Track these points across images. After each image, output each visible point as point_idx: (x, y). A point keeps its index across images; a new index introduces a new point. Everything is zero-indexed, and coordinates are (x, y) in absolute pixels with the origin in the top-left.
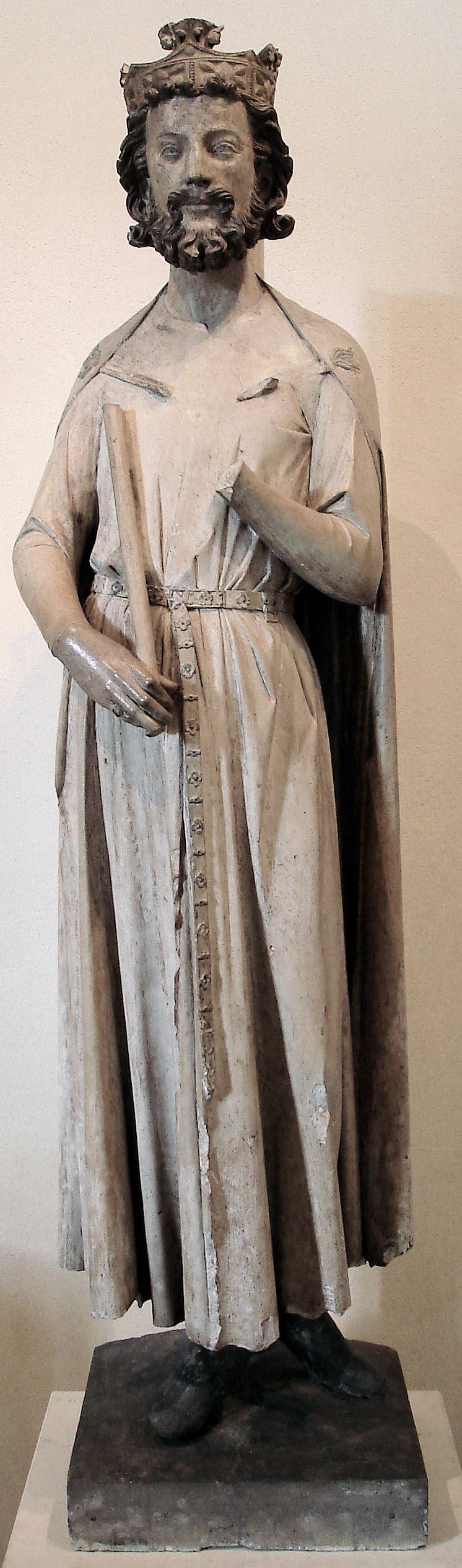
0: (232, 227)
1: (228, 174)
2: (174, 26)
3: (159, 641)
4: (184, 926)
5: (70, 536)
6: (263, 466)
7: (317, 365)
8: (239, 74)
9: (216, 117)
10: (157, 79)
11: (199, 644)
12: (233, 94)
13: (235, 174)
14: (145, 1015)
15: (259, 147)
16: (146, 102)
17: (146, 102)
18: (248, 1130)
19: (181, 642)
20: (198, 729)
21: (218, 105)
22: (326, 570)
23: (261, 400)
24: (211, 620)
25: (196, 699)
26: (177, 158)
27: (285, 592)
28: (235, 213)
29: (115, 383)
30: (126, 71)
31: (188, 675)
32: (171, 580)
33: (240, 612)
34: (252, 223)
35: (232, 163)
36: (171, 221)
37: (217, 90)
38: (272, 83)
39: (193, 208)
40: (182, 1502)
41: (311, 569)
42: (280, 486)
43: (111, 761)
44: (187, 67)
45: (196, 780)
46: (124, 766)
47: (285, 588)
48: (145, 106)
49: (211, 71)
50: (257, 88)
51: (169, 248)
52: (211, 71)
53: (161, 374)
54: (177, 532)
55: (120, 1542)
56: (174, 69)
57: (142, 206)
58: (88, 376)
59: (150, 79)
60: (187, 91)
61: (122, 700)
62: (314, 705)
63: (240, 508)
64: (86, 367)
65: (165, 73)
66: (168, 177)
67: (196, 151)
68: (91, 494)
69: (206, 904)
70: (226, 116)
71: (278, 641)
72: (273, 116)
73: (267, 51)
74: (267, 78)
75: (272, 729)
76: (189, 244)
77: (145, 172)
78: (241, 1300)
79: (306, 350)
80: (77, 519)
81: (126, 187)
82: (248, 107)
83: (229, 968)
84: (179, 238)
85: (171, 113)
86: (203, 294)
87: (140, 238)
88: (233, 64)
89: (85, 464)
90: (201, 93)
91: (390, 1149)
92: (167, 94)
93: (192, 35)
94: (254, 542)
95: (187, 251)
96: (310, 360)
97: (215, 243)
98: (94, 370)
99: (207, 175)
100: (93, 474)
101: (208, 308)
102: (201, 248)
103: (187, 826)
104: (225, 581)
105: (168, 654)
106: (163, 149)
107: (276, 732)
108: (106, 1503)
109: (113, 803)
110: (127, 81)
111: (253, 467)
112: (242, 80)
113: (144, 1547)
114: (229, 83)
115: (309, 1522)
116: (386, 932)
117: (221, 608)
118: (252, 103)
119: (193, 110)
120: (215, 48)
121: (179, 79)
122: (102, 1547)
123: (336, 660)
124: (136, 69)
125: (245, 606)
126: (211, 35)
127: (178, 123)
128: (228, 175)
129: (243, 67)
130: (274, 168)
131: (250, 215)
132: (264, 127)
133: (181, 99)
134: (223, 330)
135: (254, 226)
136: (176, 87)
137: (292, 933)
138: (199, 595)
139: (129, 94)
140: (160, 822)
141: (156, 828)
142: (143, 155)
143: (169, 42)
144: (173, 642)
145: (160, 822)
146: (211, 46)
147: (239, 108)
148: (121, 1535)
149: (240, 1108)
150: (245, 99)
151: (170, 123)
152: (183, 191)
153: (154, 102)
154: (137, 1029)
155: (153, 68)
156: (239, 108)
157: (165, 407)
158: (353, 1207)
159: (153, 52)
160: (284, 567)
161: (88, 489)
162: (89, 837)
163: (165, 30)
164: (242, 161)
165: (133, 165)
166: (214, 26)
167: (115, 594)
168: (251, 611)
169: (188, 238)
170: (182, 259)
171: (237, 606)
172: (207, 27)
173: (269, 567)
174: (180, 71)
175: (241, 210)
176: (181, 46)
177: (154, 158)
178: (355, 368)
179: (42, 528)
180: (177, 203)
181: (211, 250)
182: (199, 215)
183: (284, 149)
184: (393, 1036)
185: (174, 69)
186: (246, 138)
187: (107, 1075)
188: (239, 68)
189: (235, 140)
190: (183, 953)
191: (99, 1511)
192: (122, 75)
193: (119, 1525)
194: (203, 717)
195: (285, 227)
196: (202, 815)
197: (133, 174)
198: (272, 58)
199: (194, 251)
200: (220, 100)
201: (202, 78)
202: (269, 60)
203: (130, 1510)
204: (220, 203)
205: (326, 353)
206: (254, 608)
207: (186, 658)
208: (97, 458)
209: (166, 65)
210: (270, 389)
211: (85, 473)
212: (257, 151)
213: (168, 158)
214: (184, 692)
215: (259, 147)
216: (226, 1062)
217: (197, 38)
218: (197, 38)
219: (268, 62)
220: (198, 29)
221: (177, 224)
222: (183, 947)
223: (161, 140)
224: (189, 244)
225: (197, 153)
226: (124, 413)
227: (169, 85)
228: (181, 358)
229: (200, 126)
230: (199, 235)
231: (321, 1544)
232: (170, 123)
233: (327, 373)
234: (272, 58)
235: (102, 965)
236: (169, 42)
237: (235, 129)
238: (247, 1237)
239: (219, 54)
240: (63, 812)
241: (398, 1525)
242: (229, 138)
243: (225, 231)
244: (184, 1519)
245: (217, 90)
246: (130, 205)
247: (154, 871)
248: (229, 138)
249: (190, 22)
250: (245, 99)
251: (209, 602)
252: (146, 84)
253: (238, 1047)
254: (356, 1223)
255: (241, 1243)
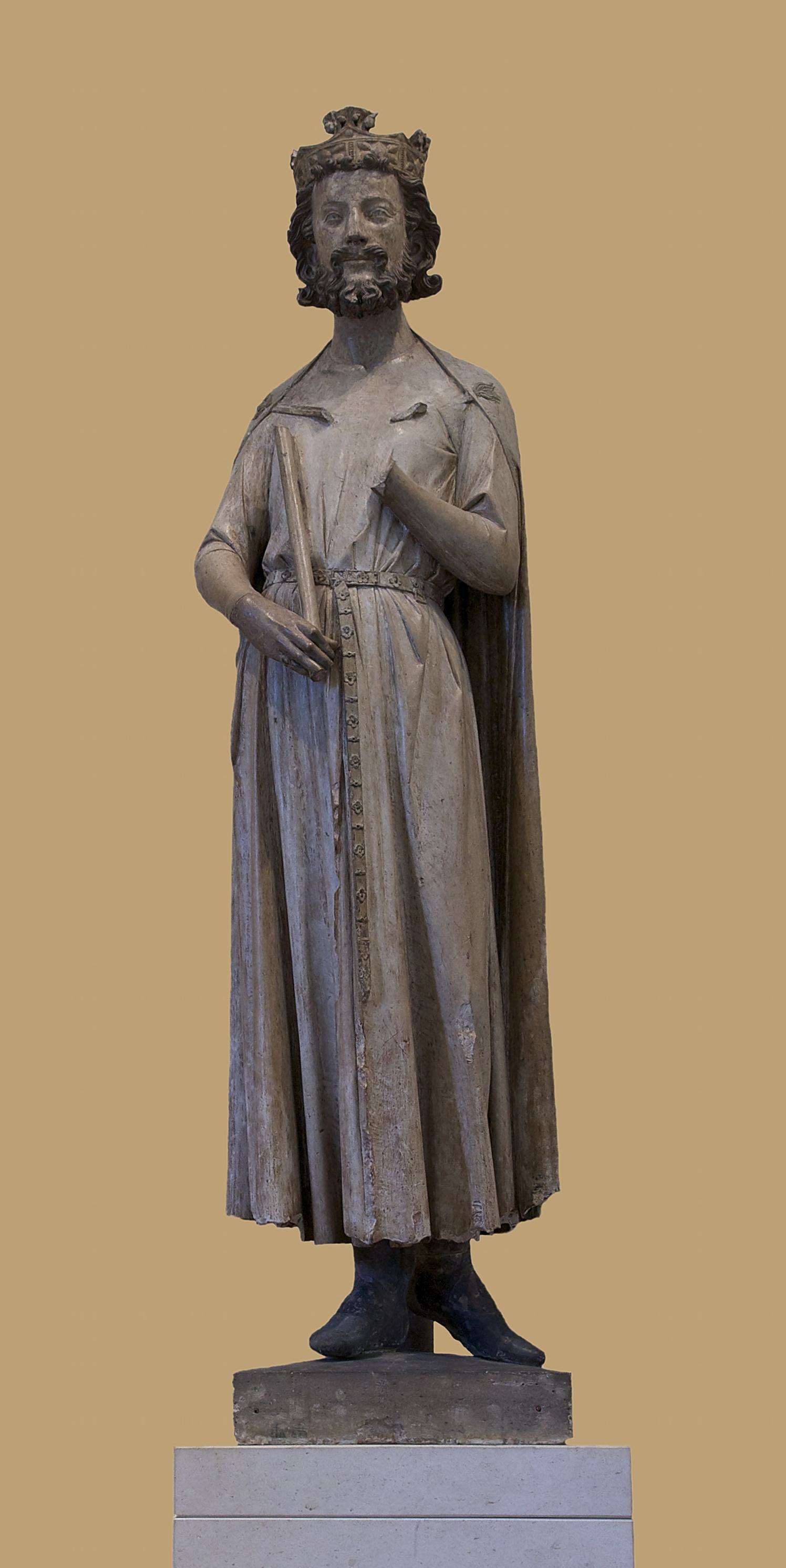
0: (386, 278)
1: (382, 234)
2: (336, 114)
3: (323, 613)
4: (343, 851)
5: (245, 545)
6: (414, 473)
7: (462, 396)
8: (393, 152)
9: (372, 187)
10: (322, 157)
11: (357, 613)
12: (386, 168)
13: (388, 235)
14: (309, 945)
15: (410, 214)
16: (312, 177)
17: (312, 177)
18: (401, 1034)
19: (341, 610)
20: (356, 680)
21: (373, 177)
22: (467, 555)
23: (411, 422)
24: (366, 602)
25: (354, 656)
26: (338, 223)
27: (432, 582)
28: (389, 267)
29: (284, 418)
30: (295, 155)
31: (346, 636)
32: (333, 562)
33: (393, 592)
34: (404, 276)
35: (385, 226)
36: (333, 275)
37: (371, 164)
38: (421, 162)
39: (352, 262)
40: (340, 1394)
41: (454, 554)
42: (429, 490)
43: (280, 720)
44: (347, 146)
45: (354, 722)
46: (292, 722)
47: (433, 578)
48: (312, 181)
49: (368, 149)
50: (407, 165)
51: (332, 298)
52: (368, 149)
53: (326, 404)
54: (335, 517)
55: (282, 1435)
56: (336, 148)
57: (309, 271)
58: (260, 417)
59: (315, 158)
60: (347, 166)
61: (291, 647)
62: (458, 673)
63: (392, 503)
64: (260, 410)
65: (328, 153)
66: (330, 238)
67: (356, 215)
68: (263, 512)
69: (362, 829)
70: (379, 187)
71: (426, 618)
72: (421, 189)
73: (418, 134)
74: (417, 157)
75: (421, 688)
76: (349, 292)
77: (311, 239)
78: (394, 1195)
79: (452, 385)
80: (252, 533)
81: (296, 256)
82: (399, 180)
83: (383, 888)
84: (341, 289)
85: (333, 185)
86: (362, 341)
87: (308, 298)
88: (386, 144)
89: (258, 487)
90: (359, 168)
91: (537, 1093)
92: (330, 169)
93: (351, 120)
94: (405, 535)
95: (348, 297)
96: (456, 392)
97: (371, 291)
98: (266, 411)
99: (364, 234)
100: (266, 495)
101: (367, 353)
102: (359, 296)
103: (346, 762)
104: (379, 564)
105: (329, 621)
106: (327, 216)
107: (424, 694)
108: (268, 1394)
109: (282, 756)
110: (296, 164)
111: (404, 468)
112: (395, 157)
113: (304, 1440)
114: (382, 159)
115: (459, 1414)
116: (529, 890)
117: (376, 586)
118: (402, 176)
119: (352, 182)
120: (371, 131)
121: (340, 156)
122: (265, 1440)
123: (484, 661)
124: (304, 151)
125: (396, 585)
126: (367, 120)
127: (339, 193)
128: (382, 236)
129: (394, 146)
130: (424, 233)
131: (401, 270)
132: (414, 197)
133: (342, 173)
134: (380, 369)
135: (406, 279)
136: (338, 163)
137: (439, 866)
138: (356, 574)
139: (298, 173)
140: (323, 767)
141: (319, 772)
142: (310, 224)
143: (332, 127)
144: (336, 612)
145: (323, 767)
146: (368, 129)
147: (391, 180)
148: (283, 1427)
149: (393, 1010)
150: (396, 173)
151: (333, 193)
152: (344, 249)
153: (319, 177)
154: (301, 957)
155: (319, 149)
156: (391, 180)
157: (329, 431)
158: (505, 1159)
159: (319, 136)
160: (433, 558)
161: (261, 505)
162: (260, 793)
163: (329, 118)
164: (394, 224)
165: (301, 234)
166: (370, 113)
167: (284, 581)
168: (402, 591)
169: (349, 288)
170: (343, 306)
171: (391, 586)
172: (364, 114)
173: (418, 557)
174: (342, 150)
175: (395, 266)
176: (342, 130)
177: (319, 224)
178: (496, 399)
179: (222, 538)
180: (338, 259)
181: (367, 296)
182: (358, 269)
183: (432, 217)
184: (537, 987)
185: (336, 148)
186: (398, 206)
187: (274, 999)
188: (391, 147)
189: (388, 206)
190: (342, 874)
191: (262, 1402)
192: (292, 158)
193: (280, 1417)
194: (359, 669)
195: (435, 285)
196: (361, 799)
197: (301, 241)
198: (421, 140)
199: (353, 298)
200: (375, 174)
201: (359, 155)
202: (419, 143)
203: (291, 1401)
204: (377, 258)
205: (469, 387)
206: (404, 588)
207: (345, 622)
208: (269, 482)
209: (328, 146)
210: (419, 413)
211: (259, 493)
212: (408, 218)
213: (331, 223)
214: (344, 649)
215: (410, 214)
216: (380, 971)
217: (356, 123)
218: (356, 123)
219: (417, 144)
220: (356, 116)
221: (339, 277)
222: (342, 869)
223: (325, 208)
224: (349, 292)
225: (356, 216)
226: (293, 438)
227: (331, 161)
228: (343, 392)
229: (358, 194)
230: (358, 284)
231: (471, 1437)
232: (333, 193)
233: (471, 402)
234: (421, 140)
235: (271, 902)
236: (332, 127)
237: (388, 197)
238: (400, 1133)
239: (374, 136)
240: (237, 778)
241: (545, 1418)
242: (383, 205)
243: (380, 282)
244: (342, 1411)
245: (371, 164)
246: (299, 271)
247: (317, 813)
248: (383, 205)
249: (349, 110)
250: (396, 173)
251: (365, 580)
252: (312, 163)
253: (390, 959)
254: (509, 1174)
255: (394, 1139)
